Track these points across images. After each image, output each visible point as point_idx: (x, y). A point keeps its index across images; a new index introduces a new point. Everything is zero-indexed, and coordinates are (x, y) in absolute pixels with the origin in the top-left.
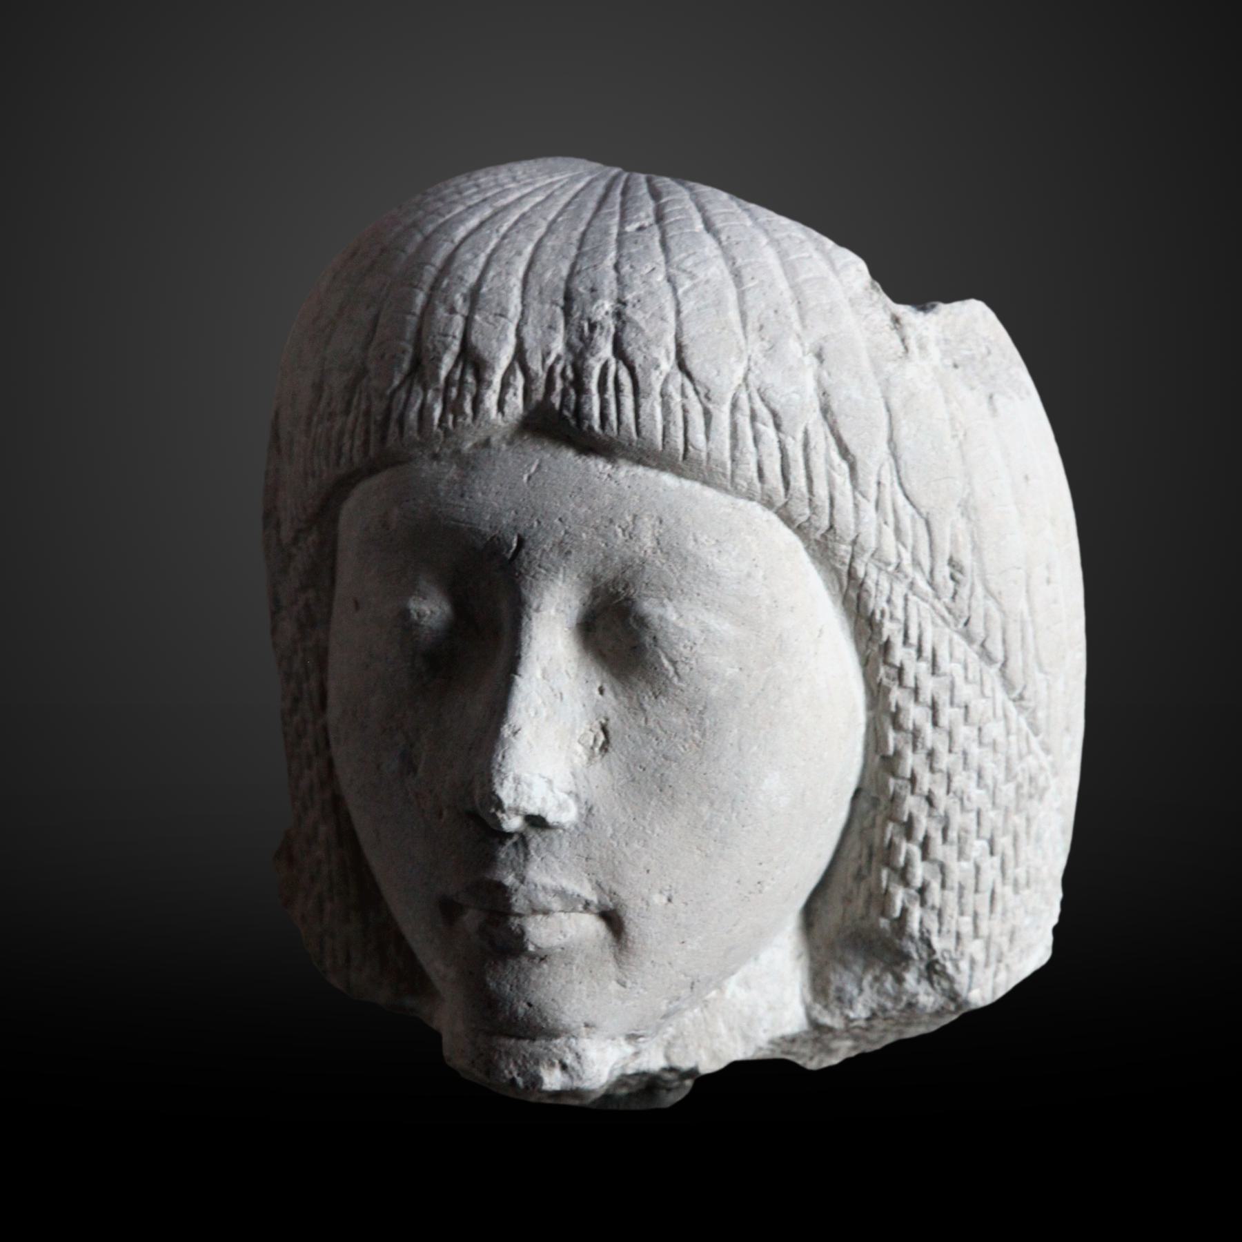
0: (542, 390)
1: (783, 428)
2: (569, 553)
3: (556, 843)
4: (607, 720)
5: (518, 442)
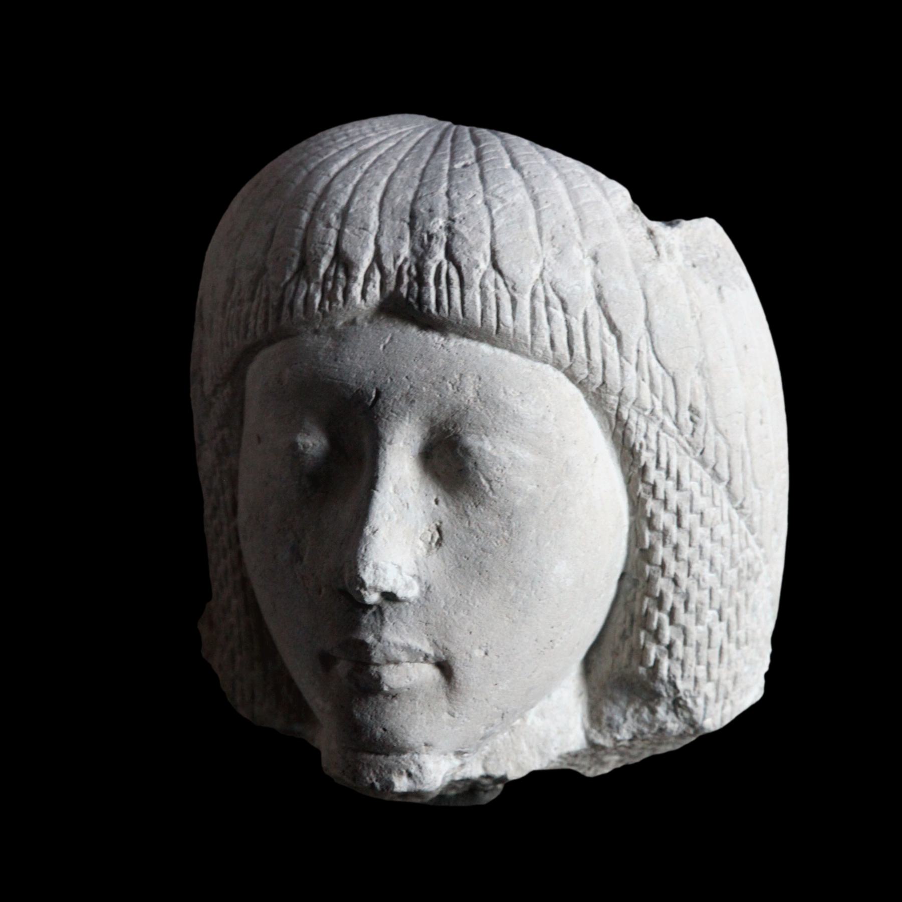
0: (393, 283)
1: (569, 311)
2: (413, 401)
3: (404, 612)
4: (441, 523)
5: (376, 321)
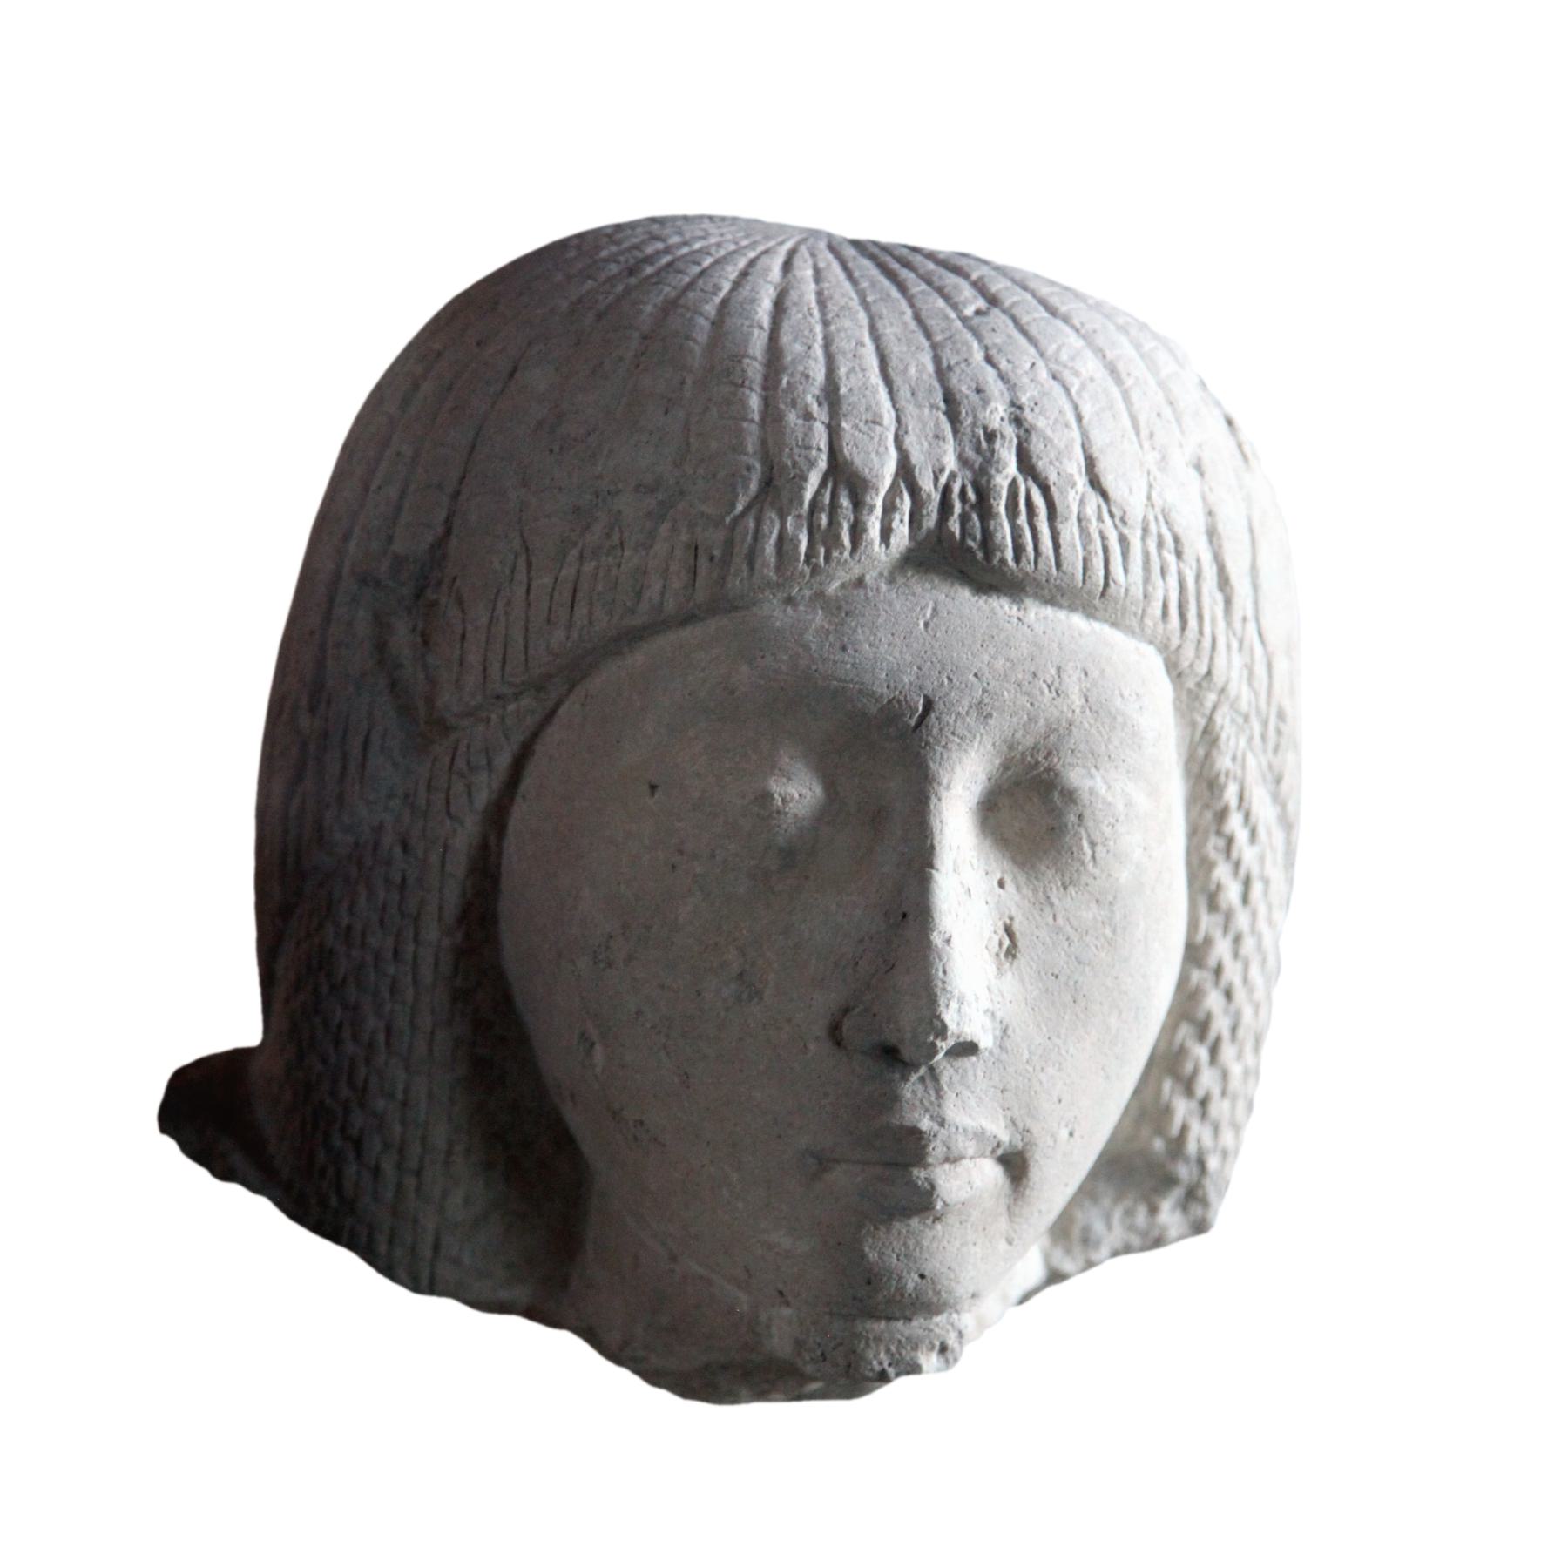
0: (935, 515)
1: (1185, 557)
2: (990, 715)
3: (970, 1073)
4: (1011, 919)
5: (901, 580)
